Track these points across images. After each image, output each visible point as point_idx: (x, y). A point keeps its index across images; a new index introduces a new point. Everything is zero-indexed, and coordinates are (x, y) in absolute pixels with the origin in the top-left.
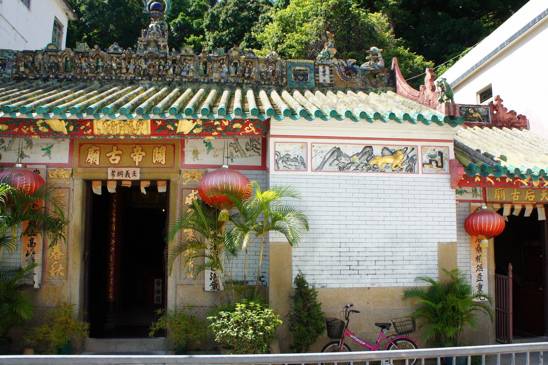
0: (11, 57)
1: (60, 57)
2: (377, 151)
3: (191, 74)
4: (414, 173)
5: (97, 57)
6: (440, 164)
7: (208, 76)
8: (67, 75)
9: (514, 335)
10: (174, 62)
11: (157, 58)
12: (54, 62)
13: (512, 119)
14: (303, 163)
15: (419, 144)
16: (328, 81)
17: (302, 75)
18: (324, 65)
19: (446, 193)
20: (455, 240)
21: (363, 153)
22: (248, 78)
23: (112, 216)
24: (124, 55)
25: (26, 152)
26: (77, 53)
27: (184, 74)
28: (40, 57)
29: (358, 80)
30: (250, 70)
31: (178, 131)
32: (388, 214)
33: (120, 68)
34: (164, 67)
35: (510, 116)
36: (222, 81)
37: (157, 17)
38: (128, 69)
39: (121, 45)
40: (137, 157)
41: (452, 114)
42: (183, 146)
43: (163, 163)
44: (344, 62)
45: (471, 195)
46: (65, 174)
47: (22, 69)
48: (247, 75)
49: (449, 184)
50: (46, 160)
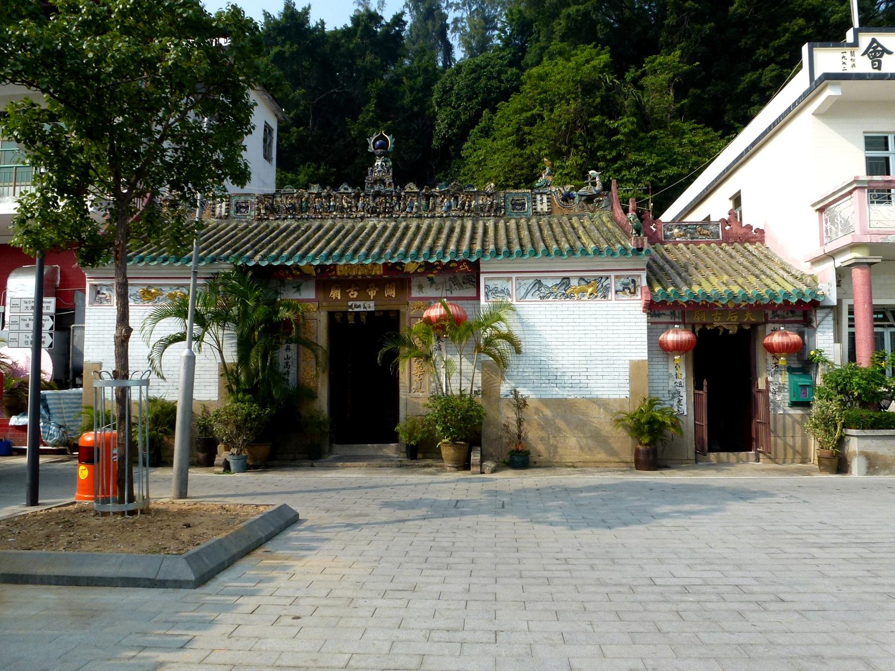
5: (328, 197)
6: (632, 290)
10: (399, 198)
13: (746, 234)
14: (509, 294)
15: (613, 274)
17: (520, 205)
21: (562, 284)
22: (468, 211)
29: (576, 205)
32: (583, 336)
34: (390, 204)
35: (745, 231)
38: (357, 207)
39: (350, 185)
42: (410, 282)
44: (561, 189)
46: (313, 306)
47: (263, 211)
50: (297, 296)
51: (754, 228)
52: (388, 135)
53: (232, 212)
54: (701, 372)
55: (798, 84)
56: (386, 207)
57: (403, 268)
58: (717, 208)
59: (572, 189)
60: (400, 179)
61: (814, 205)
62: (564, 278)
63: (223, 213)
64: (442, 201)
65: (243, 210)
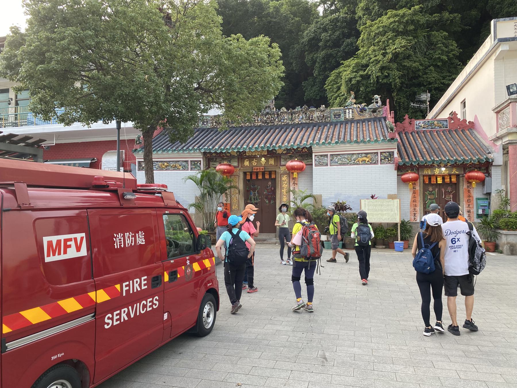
3: (285, 121)
10: (278, 114)
17: (338, 115)
27: (282, 121)
30: (312, 115)
33: (255, 121)
44: (359, 106)
47: (214, 124)
51: (468, 121)
55: (488, 44)
59: (365, 105)
60: (278, 107)
64: (298, 116)
65: (205, 123)
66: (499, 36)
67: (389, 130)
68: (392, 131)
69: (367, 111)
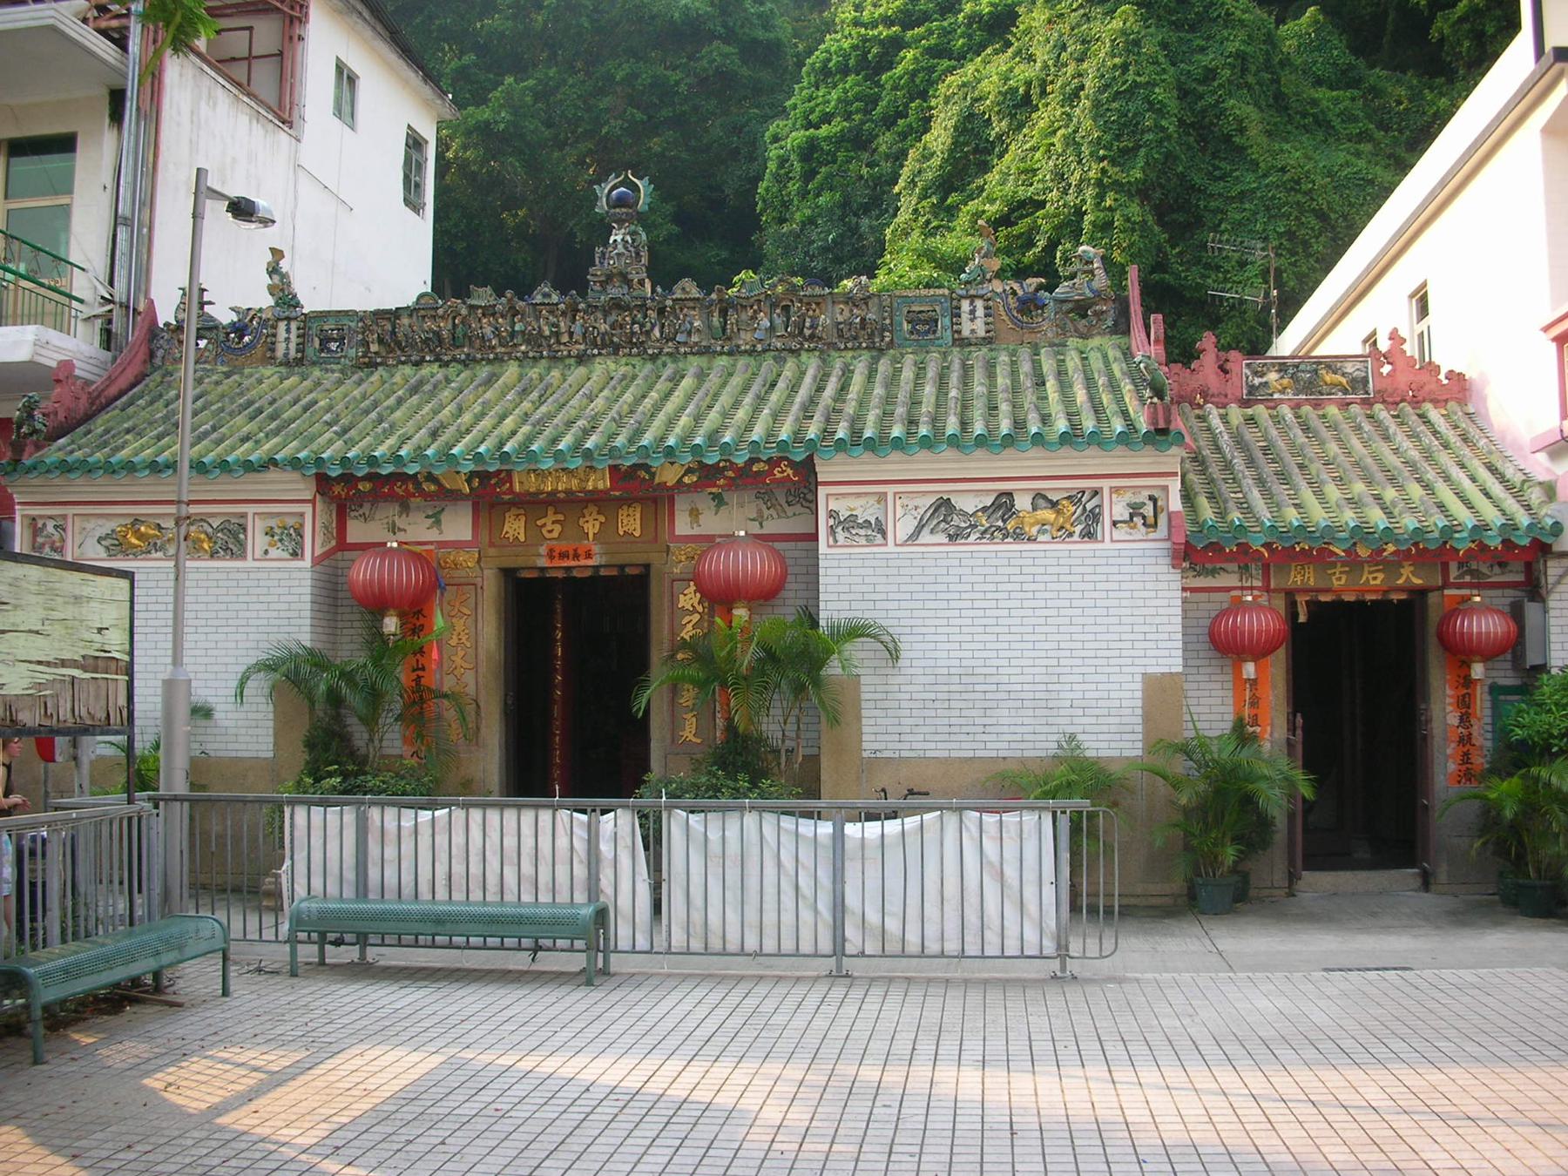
0: (353, 325)
1: (442, 317)
2: (1023, 503)
3: (695, 338)
4: (1096, 541)
7: (729, 339)
8: (457, 352)
9: (1305, 856)
10: (661, 312)
11: (627, 308)
12: (431, 330)
15: (1105, 484)
16: (981, 333)
18: (972, 298)
19: (1160, 577)
20: (1180, 669)
21: (996, 506)
23: (563, 658)
24: (562, 306)
25: (400, 522)
26: (472, 308)
28: (405, 321)
29: (1046, 324)
31: (657, 480)
33: (557, 335)
34: (642, 326)
36: (759, 347)
37: (624, 221)
38: (571, 334)
40: (590, 525)
41: (1162, 425)
43: (637, 534)
44: (1016, 286)
45: (1237, 576)
46: (468, 559)
47: (374, 348)
48: (807, 332)
49: (1168, 560)
50: (433, 535)
52: (640, 178)
53: (310, 352)
54: (1312, 694)
55: (1516, 62)
56: (633, 333)
57: (653, 475)
58: (1384, 312)
59: (1040, 287)
60: (664, 274)
61: (1546, 329)
62: (1002, 494)
63: (293, 353)
64: (754, 318)
65: (333, 346)
66: (1555, 38)
67: (1148, 393)
68: (1161, 398)
69: (1050, 312)
